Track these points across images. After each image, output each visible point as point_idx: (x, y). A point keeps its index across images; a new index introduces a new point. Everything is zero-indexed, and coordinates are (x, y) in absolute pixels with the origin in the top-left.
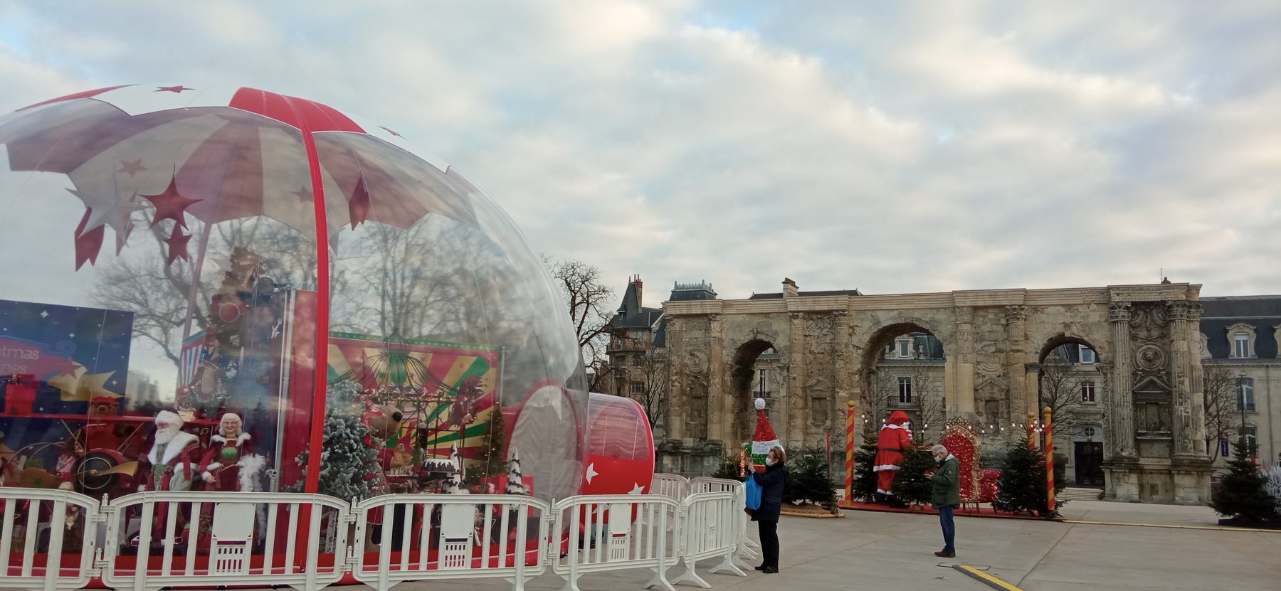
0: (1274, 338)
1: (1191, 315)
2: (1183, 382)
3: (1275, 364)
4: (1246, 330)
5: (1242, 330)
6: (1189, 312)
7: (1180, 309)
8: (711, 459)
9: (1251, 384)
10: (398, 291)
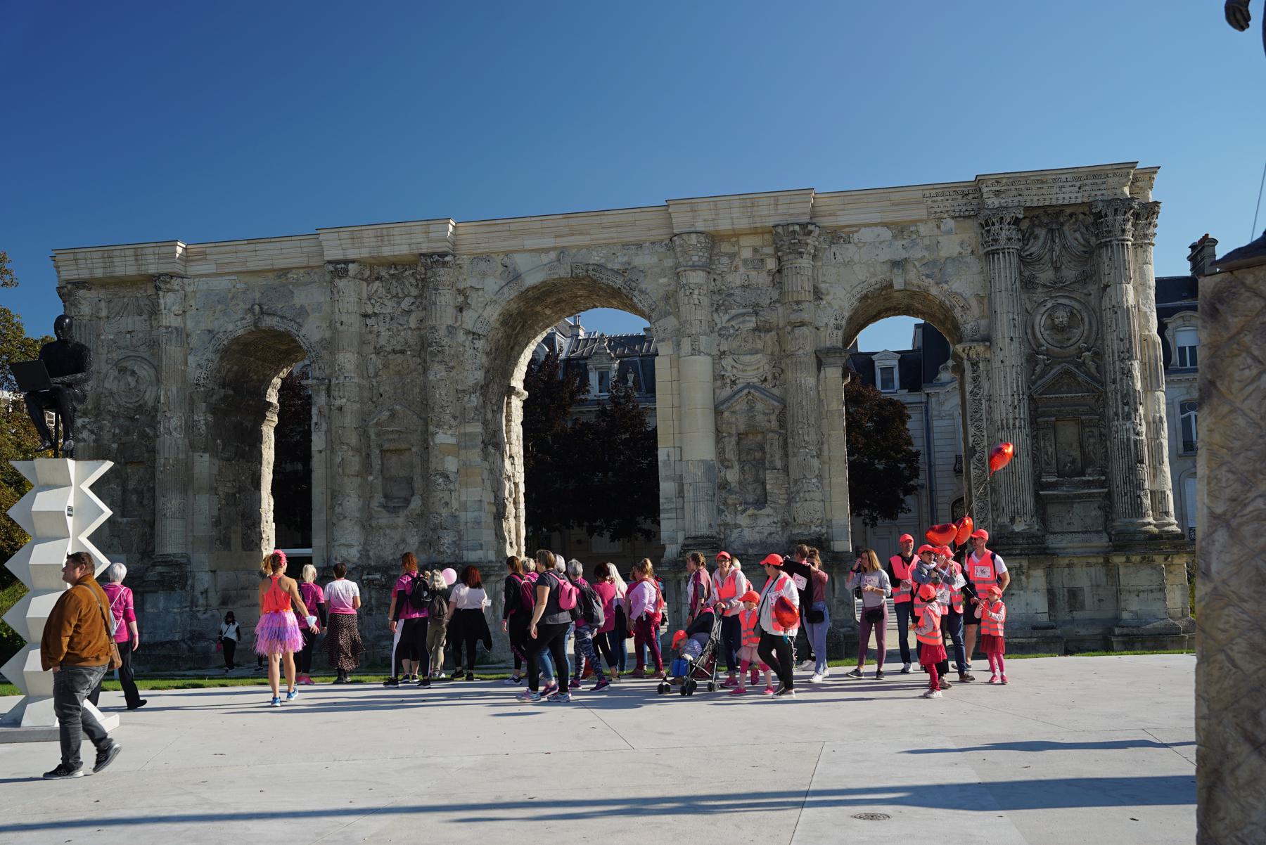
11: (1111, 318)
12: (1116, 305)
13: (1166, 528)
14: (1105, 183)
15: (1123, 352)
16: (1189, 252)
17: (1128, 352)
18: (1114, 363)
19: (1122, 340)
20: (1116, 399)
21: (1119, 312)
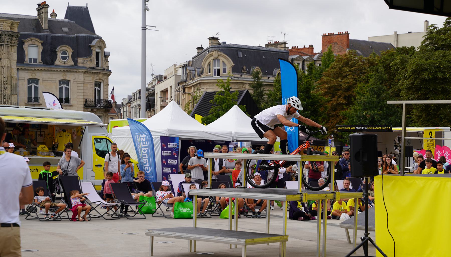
0: (23, 48)
1: (13, 41)
2: (7, 88)
3: (23, 68)
4: (36, 43)
5: (33, 43)
6: (12, 39)
7: (7, 37)
8: (42, 146)
9: (37, 83)
10: (349, 73)
11: (2, 70)
12: (4, 66)
13: (307, 180)
14: (2, 25)
15: (5, 82)
16: (37, 7)
17: (6, 82)
18: (2, 85)
19: (5, 78)
20: (2, 97)
21: (4, 68)
